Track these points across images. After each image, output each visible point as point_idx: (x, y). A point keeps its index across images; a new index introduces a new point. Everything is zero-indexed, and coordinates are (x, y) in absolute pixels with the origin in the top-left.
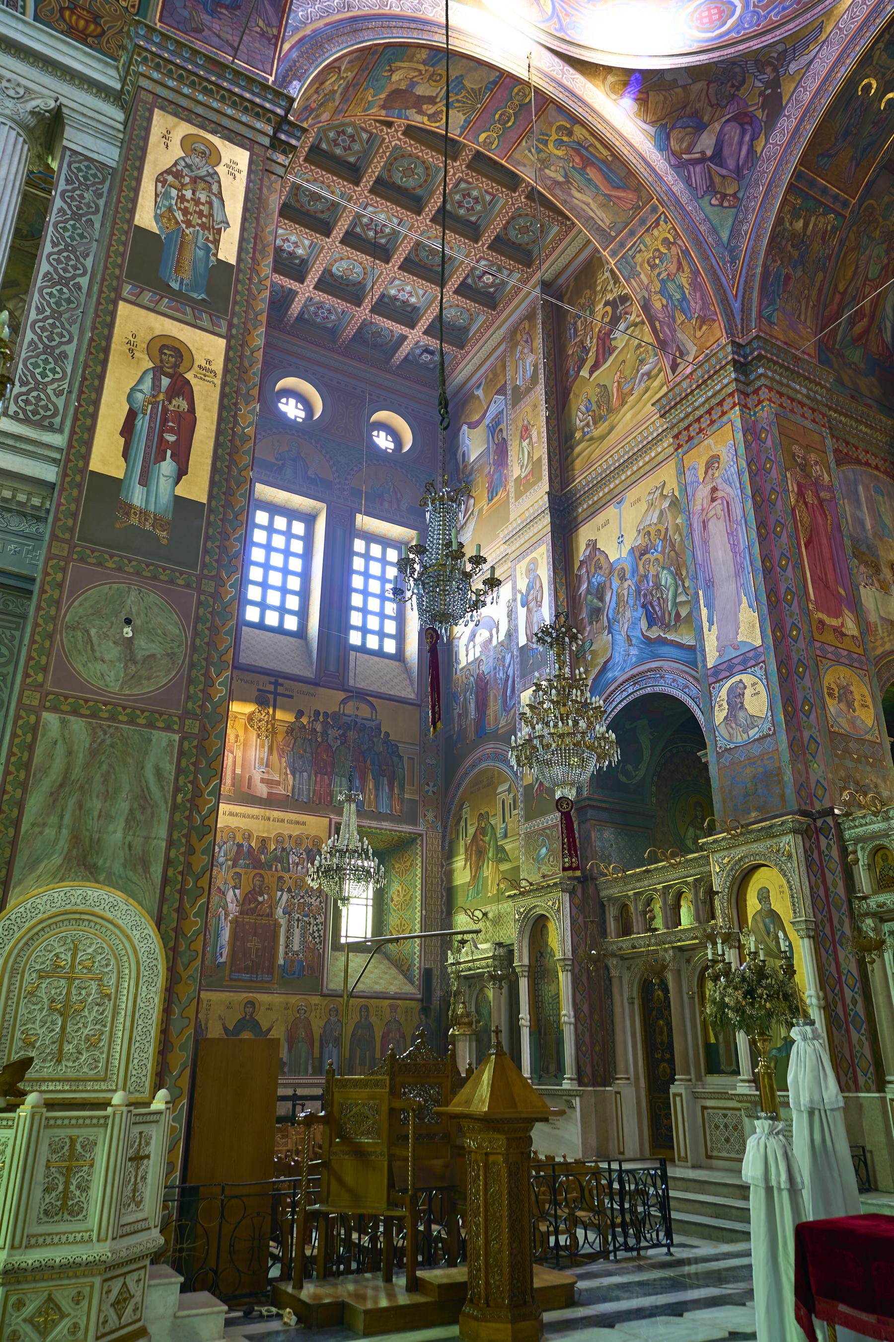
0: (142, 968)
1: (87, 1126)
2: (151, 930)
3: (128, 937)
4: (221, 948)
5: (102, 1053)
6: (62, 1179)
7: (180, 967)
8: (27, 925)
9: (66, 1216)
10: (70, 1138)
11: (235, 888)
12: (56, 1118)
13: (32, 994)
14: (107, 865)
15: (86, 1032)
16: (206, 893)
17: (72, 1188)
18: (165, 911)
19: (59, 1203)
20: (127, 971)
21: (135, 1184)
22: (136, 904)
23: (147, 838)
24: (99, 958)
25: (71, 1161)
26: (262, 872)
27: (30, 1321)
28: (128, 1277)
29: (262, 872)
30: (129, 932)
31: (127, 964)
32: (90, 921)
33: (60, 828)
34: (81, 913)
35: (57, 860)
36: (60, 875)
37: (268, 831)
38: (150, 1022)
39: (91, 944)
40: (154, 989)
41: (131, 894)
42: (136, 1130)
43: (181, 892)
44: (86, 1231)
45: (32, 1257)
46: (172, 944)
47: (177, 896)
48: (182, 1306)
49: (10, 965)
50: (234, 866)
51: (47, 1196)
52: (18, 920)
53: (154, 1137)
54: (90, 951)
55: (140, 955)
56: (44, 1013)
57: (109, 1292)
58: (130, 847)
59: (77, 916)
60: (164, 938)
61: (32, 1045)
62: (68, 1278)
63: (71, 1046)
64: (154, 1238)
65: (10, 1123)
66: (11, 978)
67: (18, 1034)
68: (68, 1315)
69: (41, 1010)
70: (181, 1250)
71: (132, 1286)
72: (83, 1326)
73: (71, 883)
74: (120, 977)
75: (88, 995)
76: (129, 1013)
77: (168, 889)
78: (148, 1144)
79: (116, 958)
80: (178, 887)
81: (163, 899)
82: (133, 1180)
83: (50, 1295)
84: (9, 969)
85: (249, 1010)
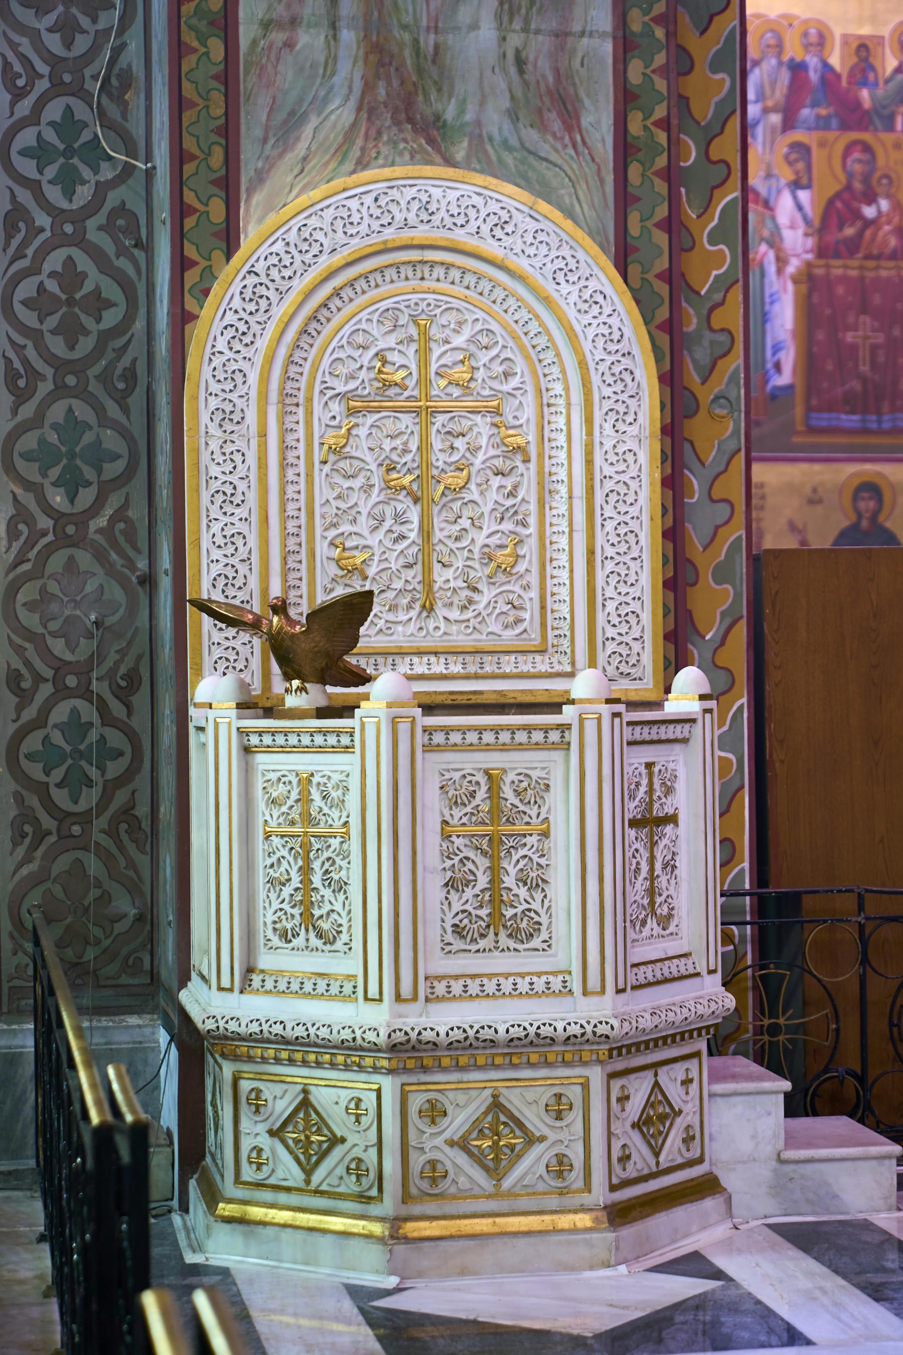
0: (596, 379)
1: (520, 747)
2: (605, 280)
3: (546, 300)
4: (777, 348)
5: (527, 587)
6: (483, 863)
7: (693, 377)
8: (299, 285)
9: (504, 941)
10: (487, 772)
11: (796, 185)
12: (447, 730)
13: (337, 451)
14: (469, 117)
15: (481, 539)
16: (737, 174)
17: (509, 881)
18: (634, 228)
19: (484, 912)
20: (558, 388)
21: (652, 877)
22: (557, 215)
23: (561, 35)
24: (484, 357)
25: (497, 825)
26: (866, 136)
27: (462, 1144)
28: (663, 1071)
29: (866, 136)
30: (550, 287)
31: (555, 370)
32: (448, 266)
33: (334, 26)
34: (422, 247)
35: (341, 113)
36: (355, 152)
37: (874, 19)
38: (634, 511)
39: (460, 324)
40: (633, 430)
41: (544, 191)
42: (638, 758)
43: (670, 174)
44: (555, 973)
45: (443, 1020)
46: (663, 313)
47: (661, 187)
48: (791, 1141)
49: (274, 385)
50: (788, 124)
51: (454, 896)
52: (274, 273)
53: (681, 773)
54: (459, 341)
55: (587, 346)
56: (374, 498)
57: (624, 1099)
58: (520, 62)
59: (414, 255)
60: (642, 299)
61: (359, 571)
62: (531, 1065)
63: (449, 573)
64: (708, 996)
65: (345, 740)
66: (284, 414)
67: (322, 549)
68: (542, 1139)
69: (368, 488)
70: (774, 1030)
71: (674, 1092)
72: (578, 1160)
73: (387, 172)
74: (542, 406)
75: (473, 450)
76: (579, 490)
77: (634, 171)
78: (669, 791)
79: (527, 357)
80: (662, 161)
81: (624, 198)
82: (645, 868)
83: (495, 1096)
84: (274, 396)
85: (867, 505)
